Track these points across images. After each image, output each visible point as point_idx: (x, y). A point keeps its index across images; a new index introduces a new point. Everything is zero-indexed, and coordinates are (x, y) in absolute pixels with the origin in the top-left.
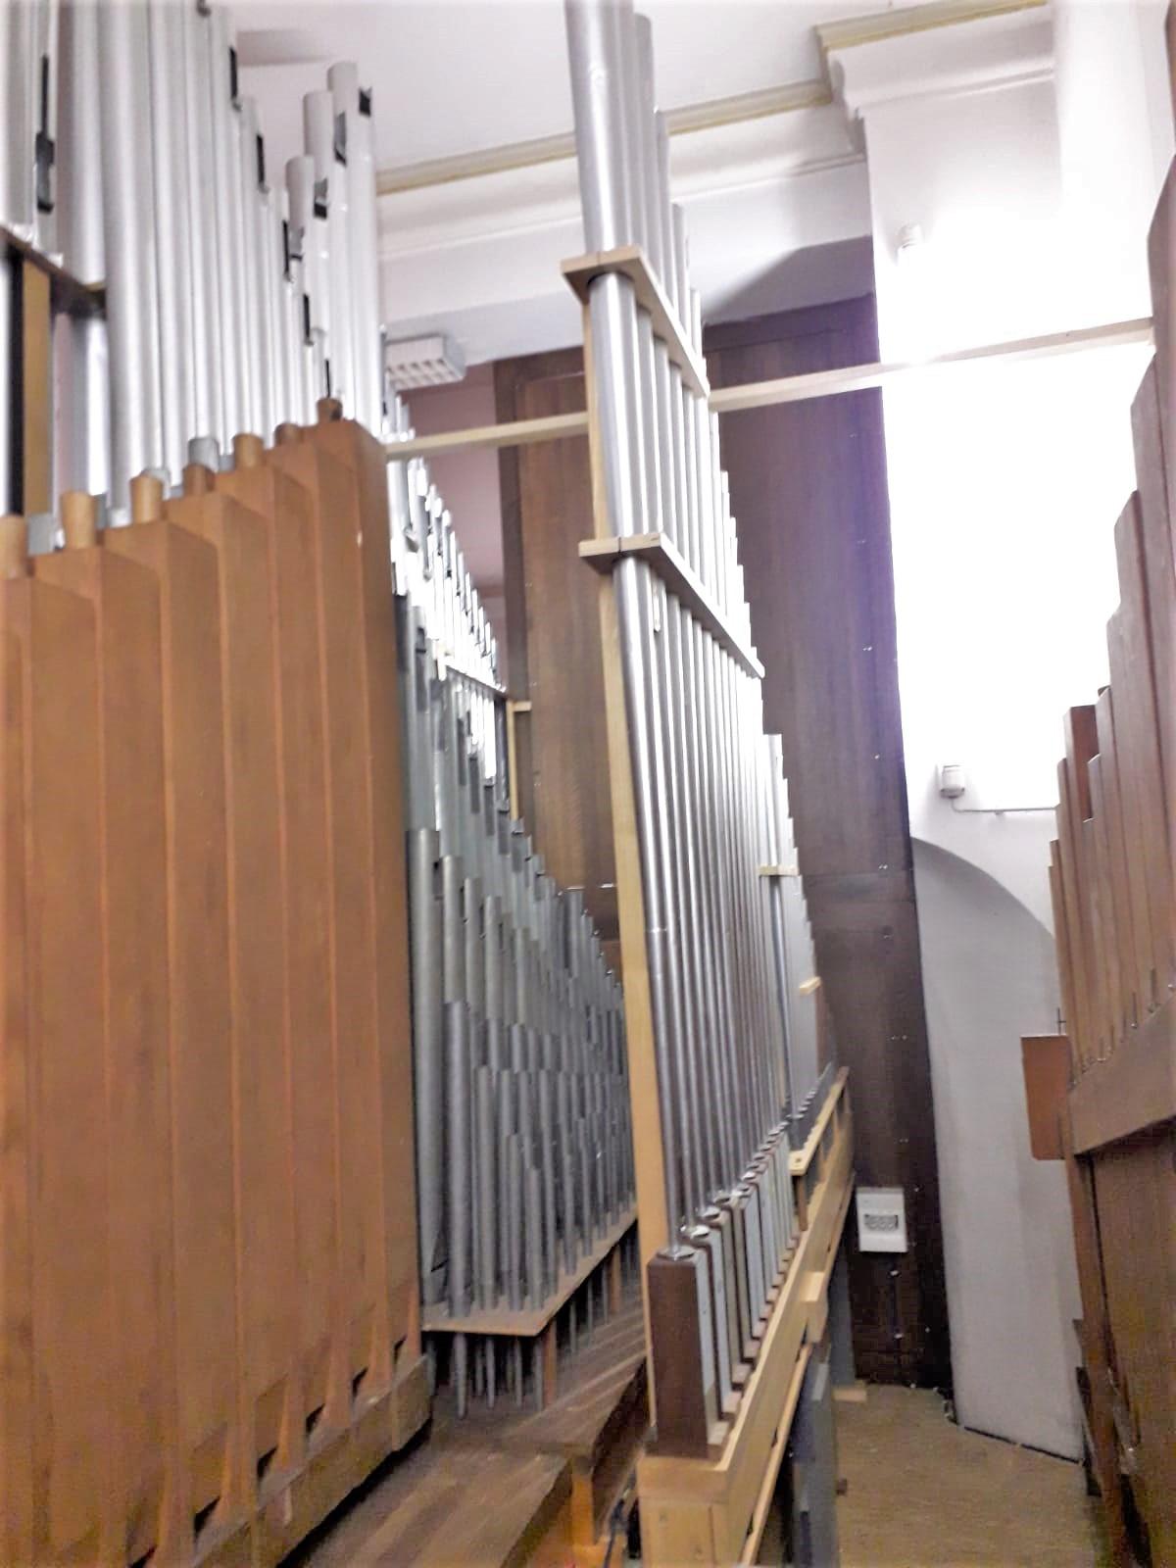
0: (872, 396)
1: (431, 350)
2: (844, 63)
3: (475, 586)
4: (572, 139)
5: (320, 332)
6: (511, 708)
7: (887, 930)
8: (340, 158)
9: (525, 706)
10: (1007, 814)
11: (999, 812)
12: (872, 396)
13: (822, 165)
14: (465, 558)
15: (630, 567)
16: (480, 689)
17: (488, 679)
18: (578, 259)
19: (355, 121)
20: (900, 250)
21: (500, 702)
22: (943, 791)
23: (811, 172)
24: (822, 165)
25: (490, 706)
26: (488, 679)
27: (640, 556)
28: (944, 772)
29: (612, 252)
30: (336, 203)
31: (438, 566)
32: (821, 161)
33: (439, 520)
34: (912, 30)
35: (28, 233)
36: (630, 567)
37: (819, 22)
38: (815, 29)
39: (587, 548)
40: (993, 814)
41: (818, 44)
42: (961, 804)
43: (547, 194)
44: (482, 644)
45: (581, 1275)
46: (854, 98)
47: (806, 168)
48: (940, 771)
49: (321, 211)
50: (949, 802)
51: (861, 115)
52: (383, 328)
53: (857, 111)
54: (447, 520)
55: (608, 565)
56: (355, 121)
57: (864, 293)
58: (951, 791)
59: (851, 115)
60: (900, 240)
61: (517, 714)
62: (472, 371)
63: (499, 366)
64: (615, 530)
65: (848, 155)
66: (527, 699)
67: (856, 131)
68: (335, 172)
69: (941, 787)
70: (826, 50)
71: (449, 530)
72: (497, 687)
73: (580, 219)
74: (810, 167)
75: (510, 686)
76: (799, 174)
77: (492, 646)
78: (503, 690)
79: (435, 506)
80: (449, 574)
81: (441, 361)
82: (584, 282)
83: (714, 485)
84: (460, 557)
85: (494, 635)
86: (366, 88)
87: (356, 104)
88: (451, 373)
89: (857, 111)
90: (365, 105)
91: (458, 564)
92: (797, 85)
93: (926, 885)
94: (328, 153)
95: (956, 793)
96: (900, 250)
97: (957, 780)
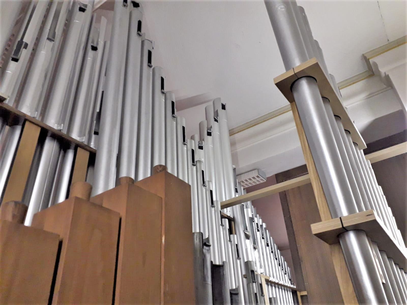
1: (255, 174)
3: (279, 248)
5: (200, 161)
6: (299, 294)
8: (216, 120)
9: (305, 293)
14: (273, 238)
15: (352, 238)
16: (285, 288)
17: (288, 284)
19: (221, 111)
21: (294, 292)
23: (372, 97)
24: (378, 93)
25: (290, 295)
26: (288, 284)
27: (358, 229)
29: (299, 66)
30: (215, 132)
31: (261, 243)
32: (378, 91)
33: (262, 226)
34: (398, 46)
35: (83, 139)
36: (352, 238)
37: (364, 53)
38: (363, 55)
39: (316, 228)
41: (365, 59)
44: (284, 270)
45: (281, 19)
46: (383, 70)
47: (370, 96)
49: (209, 134)
51: (387, 74)
52: (234, 166)
53: (385, 73)
54: (264, 225)
55: (336, 237)
56: (221, 111)
57: (402, 131)
59: (383, 75)
61: (302, 297)
62: (268, 179)
63: (276, 175)
64: (333, 211)
65: (386, 88)
66: (305, 290)
67: (387, 82)
68: (215, 126)
70: (369, 59)
71: (266, 229)
72: (292, 286)
73: (296, 127)
75: (297, 286)
77: (288, 270)
78: (295, 287)
79: (258, 220)
80: (268, 245)
81: (258, 177)
82: (288, 87)
83: (377, 192)
84: (271, 238)
85: (288, 265)
86: (224, 104)
87: (221, 107)
88: (262, 180)
89: (385, 73)
90: (224, 107)
91: (271, 240)
92: (361, 74)
94: (213, 120)
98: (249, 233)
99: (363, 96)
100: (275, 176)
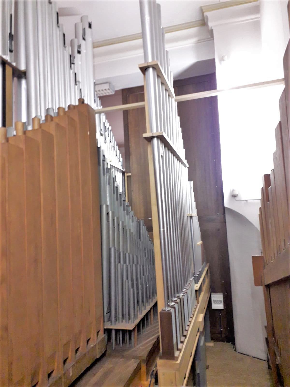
0: (215, 98)
1: (106, 86)
2: (208, 16)
3: (117, 145)
4: (141, 34)
5: (79, 82)
6: (126, 175)
7: (219, 230)
8: (84, 39)
9: (130, 174)
10: (248, 201)
11: (246, 200)
12: (215, 98)
13: (203, 41)
14: (115, 138)
15: (155, 140)
16: (118, 170)
17: (120, 168)
18: (142, 64)
19: (88, 30)
20: (222, 62)
21: (123, 173)
22: (233, 195)
24: (203, 41)
25: (121, 174)
26: (120, 168)
27: (158, 137)
28: (233, 191)
29: (151, 62)
30: (83, 50)
31: (108, 140)
32: (202, 40)
33: (108, 128)
34: (225, 7)
35: (7, 57)
36: (155, 140)
37: (202, 5)
38: (201, 7)
39: (145, 135)
40: (245, 201)
41: (202, 11)
42: (237, 198)
43: (135, 48)
44: (119, 159)
46: (211, 24)
47: (199, 42)
48: (232, 190)
49: (79, 52)
50: (234, 198)
51: (212, 28)
52: (94, 81)
53: (211, 27)
54: (110, 128)
55: (150, 139)
56: (88, 30)
57: (213, 72)
58: (235, 195)
59: (210, 28)
60: (222, 59)
61: (128, 176)
62: (116, 92)
63: (123, 90)
64: (152, 131)
65: (209, 38)
66: (130, 172)
67: (211, 32)
68: (83, 43)
69: (232, 194)
70: (204, 12)
71: (111, 131)
72: (123, 170)
73: (143, 54)
74: (200, 41)
75: (126, 169)
76: (197, 43)
77: (121, 159)
78: (124, 170)
79: (107, 125)
80: (111, 142)
81: (109, 89)
82: (144, 70)
83: (176, 120)
85: (122, 157)
86: (90, 22)
87: (88, 26)
88: (111, 92)
89: (211, 27)
90: (90, 26)
91: (113, 139)
92: (197, 21)
93: (228, 218)
94: (81, 38)
95: (236, 196)
96: (222, 62)
97: (236, 193)
98: (102, 132)
99: (194, 40)
100: (121, 91)
